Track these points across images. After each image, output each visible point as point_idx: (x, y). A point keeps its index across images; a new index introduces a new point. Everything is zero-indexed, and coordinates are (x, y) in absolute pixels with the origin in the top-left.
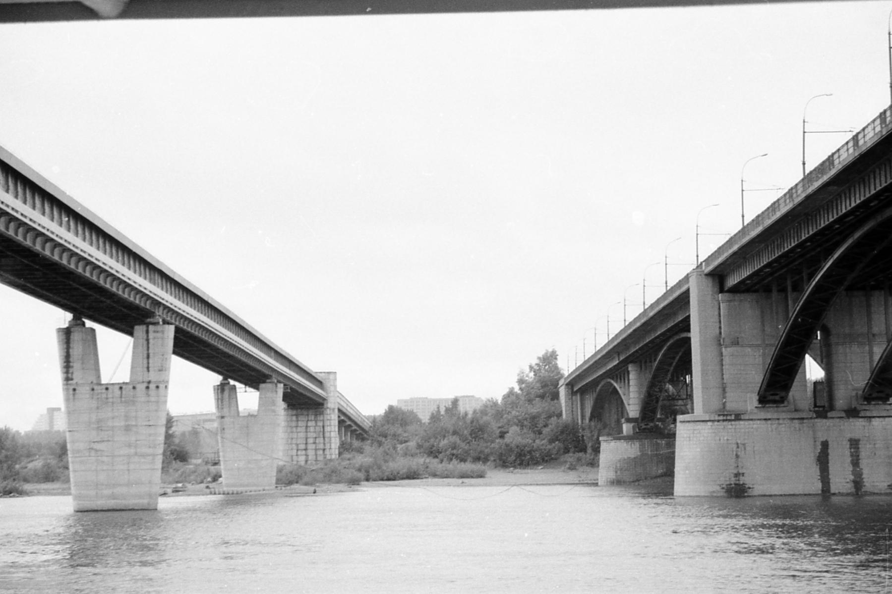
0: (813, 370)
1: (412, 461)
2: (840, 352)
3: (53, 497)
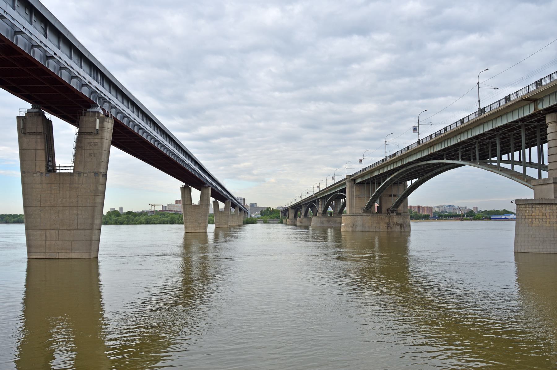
0: (377, 205)
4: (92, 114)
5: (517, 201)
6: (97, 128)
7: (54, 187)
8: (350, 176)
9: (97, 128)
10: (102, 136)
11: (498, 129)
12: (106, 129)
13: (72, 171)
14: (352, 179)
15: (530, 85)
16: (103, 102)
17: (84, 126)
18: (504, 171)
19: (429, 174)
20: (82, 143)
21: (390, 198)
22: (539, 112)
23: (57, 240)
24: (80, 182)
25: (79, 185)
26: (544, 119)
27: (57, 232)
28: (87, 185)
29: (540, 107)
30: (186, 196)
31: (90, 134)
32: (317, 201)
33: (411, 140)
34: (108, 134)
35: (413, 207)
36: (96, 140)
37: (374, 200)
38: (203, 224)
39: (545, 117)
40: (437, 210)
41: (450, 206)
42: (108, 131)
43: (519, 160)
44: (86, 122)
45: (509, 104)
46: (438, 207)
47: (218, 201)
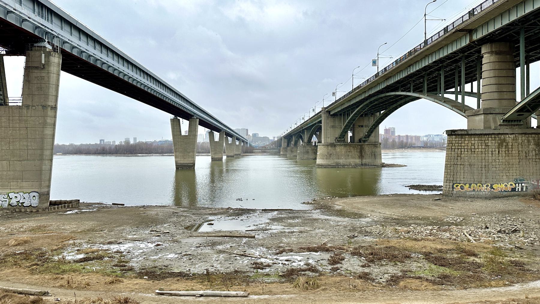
0: (350, 134)
1: (46, 156)
2: (357, 130)
3: (53, 166)
4: (39, 48)
5: (447, 131)
6: (43, 62)
7: (4, 120)
8: (326, 108)
9: (43, 62)
10: (48, 70)
11: (441, 61)
12: (53, 63)
13: (21, 104)
14: (326, 111)
15: (464, 15)
16: (52, 37)
17: (31, 61)
18: (447, 101)
19: (394, 106)
20: (29, 77)
21: (362, 128)
22: (474, 42)
23: (8, 170)
24: (28, 115)
25: (28, 118)
26: (479, 51)
27: (8, 163)
28: (36, 117)
29: (475, 38)
30: (175, 127)
31: (37, 68)
32: (303, 131)
33: (370, 72)
34: (55, 68)
35: (402, 136)
36: (43, 75)
37: (346, 130)
38: (192, 153)
39: (481, 48)
40: (425, 139)
41: (438, 135)
42: (55, 65)
43: (471, 91)
44: (32, 56)
45: (447, 35)
46: (426, 136)
47: (214, 132)
